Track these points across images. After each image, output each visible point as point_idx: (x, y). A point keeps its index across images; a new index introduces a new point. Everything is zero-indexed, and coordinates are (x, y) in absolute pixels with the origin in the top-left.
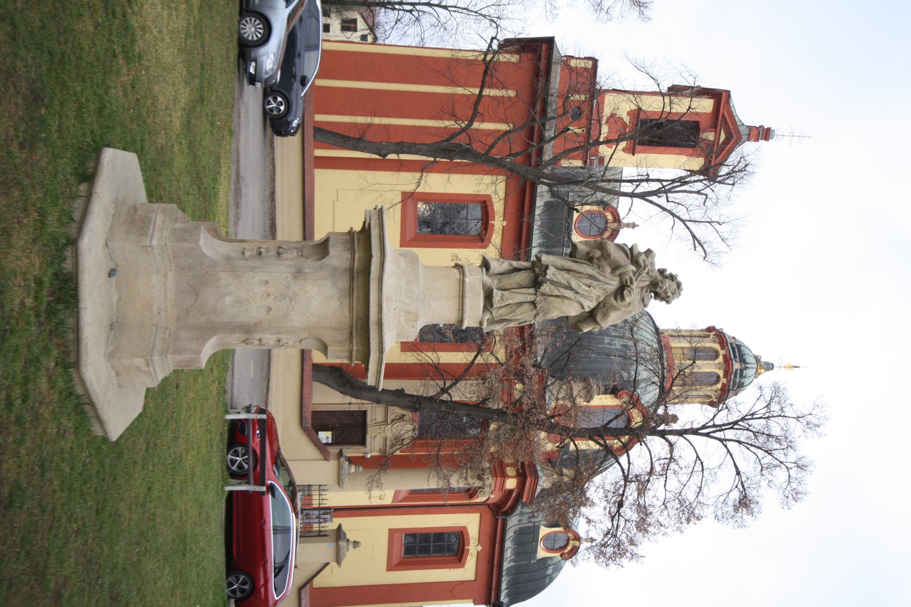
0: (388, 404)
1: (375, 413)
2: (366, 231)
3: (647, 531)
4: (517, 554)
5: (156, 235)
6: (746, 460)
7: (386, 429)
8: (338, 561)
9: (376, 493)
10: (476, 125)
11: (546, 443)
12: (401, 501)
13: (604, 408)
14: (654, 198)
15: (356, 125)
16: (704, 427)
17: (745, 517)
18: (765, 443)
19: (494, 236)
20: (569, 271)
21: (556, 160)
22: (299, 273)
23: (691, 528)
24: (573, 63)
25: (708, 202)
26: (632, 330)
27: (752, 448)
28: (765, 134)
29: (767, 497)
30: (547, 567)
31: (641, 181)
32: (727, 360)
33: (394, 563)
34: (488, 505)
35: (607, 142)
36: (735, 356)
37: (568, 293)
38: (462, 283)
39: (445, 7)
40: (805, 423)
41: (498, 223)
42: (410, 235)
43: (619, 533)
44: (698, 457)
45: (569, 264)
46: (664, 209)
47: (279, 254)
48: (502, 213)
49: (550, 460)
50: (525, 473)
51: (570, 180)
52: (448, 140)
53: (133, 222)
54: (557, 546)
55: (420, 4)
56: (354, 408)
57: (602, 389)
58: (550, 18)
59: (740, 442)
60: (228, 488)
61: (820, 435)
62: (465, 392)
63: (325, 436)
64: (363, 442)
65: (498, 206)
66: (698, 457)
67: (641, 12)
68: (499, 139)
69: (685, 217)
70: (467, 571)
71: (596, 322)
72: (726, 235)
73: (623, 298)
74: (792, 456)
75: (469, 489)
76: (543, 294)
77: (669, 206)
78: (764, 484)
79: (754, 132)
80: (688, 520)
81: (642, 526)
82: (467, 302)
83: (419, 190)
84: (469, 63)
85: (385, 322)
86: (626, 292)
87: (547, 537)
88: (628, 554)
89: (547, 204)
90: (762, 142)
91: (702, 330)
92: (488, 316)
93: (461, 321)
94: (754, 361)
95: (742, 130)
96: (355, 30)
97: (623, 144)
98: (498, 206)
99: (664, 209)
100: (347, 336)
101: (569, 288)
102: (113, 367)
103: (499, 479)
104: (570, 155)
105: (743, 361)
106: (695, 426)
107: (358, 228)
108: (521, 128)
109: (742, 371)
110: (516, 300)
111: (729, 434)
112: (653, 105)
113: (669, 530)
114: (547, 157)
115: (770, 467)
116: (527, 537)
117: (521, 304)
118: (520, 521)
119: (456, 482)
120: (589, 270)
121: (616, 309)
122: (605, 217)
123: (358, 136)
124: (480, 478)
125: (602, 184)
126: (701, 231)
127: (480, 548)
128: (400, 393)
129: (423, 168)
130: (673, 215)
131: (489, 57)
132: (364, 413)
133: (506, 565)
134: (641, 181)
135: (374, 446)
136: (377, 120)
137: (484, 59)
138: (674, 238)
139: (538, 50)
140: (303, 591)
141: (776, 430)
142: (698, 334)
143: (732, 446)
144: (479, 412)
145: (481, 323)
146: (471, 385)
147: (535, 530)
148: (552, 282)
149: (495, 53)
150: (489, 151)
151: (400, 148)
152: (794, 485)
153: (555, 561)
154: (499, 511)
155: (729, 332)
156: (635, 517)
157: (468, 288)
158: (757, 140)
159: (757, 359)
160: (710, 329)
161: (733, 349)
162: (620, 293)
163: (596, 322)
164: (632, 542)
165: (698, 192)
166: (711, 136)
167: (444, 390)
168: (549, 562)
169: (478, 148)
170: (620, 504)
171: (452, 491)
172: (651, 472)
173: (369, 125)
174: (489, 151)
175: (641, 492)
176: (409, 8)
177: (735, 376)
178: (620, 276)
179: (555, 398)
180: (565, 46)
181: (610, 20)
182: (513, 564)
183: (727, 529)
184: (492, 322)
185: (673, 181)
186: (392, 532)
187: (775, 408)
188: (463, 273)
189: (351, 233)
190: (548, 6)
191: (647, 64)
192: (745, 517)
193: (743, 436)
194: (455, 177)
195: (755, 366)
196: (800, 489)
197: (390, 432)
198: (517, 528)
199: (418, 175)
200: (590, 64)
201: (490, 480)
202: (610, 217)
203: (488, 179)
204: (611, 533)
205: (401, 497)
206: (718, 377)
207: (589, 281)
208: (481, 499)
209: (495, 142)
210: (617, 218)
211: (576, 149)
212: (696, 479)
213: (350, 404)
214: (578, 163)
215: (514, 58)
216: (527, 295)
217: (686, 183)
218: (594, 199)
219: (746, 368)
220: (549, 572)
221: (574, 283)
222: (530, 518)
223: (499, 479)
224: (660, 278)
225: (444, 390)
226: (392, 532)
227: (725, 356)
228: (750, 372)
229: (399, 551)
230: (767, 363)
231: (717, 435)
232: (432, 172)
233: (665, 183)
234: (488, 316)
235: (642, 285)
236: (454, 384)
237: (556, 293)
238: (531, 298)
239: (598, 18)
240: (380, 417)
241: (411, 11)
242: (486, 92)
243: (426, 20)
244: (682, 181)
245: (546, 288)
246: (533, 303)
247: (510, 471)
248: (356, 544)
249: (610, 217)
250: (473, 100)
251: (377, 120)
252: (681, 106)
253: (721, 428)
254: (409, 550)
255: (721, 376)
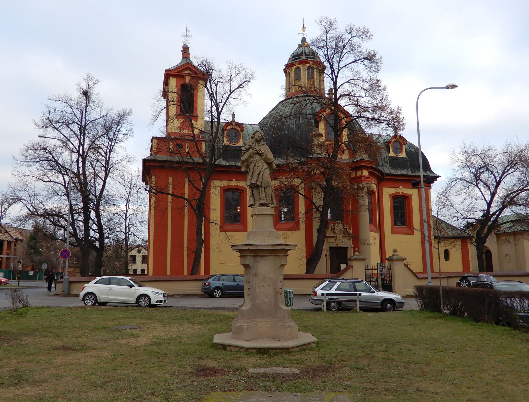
0: (325, 237)
1: (329, 243)
2: (239, 251)
3: (386, 106)
4: (404, 167)
5: (244, 325)
6: (348, 58)
7: (338, 237)
8: (403, 260)
9: (372, 241)
10: (186, 197)
11: (344, 157)
12: (377, 228)
13: (326, 129)
14: (220, 109)
15: (188, 255)
16: (333, 80)
17: (377, 58)
18: (339, 49)
19: (240, 185)
20: (252, 174)
21: (201, 155)
22: (255, 275)
23: (383, 84)
24: (155, 149)
25: (222, 80)
26: (284, 117)
27: (342, 55)
28: (186, 50)
29: (367, 46)
30: (411, 152)
31: (212, 115)
32: (301, 63)
33: (410, 231)
34: (378, 183)
35: (193, 131)
36: (299, 58)
37: (261, 175)
38: (258, 215)
39: (127, 211)
40: (329, 29)
41: (234, 183)
42: (241, 227)
43: (388, 120)
44: (347, 82)
45: (250, 175)
46: (225, 103)
47: (249, 282)
48: (229, 181)
49: (353, 153)
50: (357, 166)
51: (212, 149)
52: (195, 210)
53: (238, 332)
54: (400, 147)
55: (125, 224)
56: (328, 253)
57: (317, 129)
58: (132, 159)
59: (340, 61)
60: (358, 310)
61: (335, 21)
62: (318, 199)
63: (343, 267)
64: (346, 248)
65: (226, 183)
66: (347, 82)
67: (128, 114)
68: (194, 186)
69: (229, 93)
70: (413, 193)
71: (272, 162)
72: (237, 72)
73: (262, 153)
74: (346, 36)
75: (369, 194)
76: (261, 184)
77: (224, 101)
78: (359, 50)
79: (186, 55)
80: (379, 86)
81: (383, 108)
82: (265, 213)
83: (219, 223)
84: (157, 201)
85: (272, 244)
86: (260, 152)
87: (395, 152)
88: (398, 114)
89: (224, 160)
90: (190, 51)
91: (286, 76)
92: (270, 205)
93: (272, 215)
94: (301, 48)
95: (185, 62)
96: (135, 256)
97: (193, 122)
98: (226, 183)
99: (225, 103)
100: (278, 257)
101: (259, 174)
102: (290, 339)
103: (363, 179)
104: (199, 149)
105: (301, 54)
106: (332, 83)
107: (239, 254)
108: (187, 174)
109: (306, 55)
110: (264, 194)
111: (335, 66)
112: (173, 109)
113: (385, 94)
114: (200, 160)
115: (351, 46)
116: (395, 163)
117: (265, 192)
118: (386, 167)
119: (365, 201)
120: (252, 166)
121: (267, 155)
122: (230, 129)
123: (194, 254)
124: (363, 189)
125: (214, 135)
126: (235, 85)
127: (401, 187)
128: (319, 231)
129: (208, 222)
130: (228, 98)
131: (154, 191)
132: (331, 248)
133: (410, 173)
134: (212, 115)
135: (348, 243)
136: (186, 245)
137: (155, 194)
138: (239, 98)
139: (149, 166)
140: (419, 277)
141: (333, 44)
142: (288, 78)
143: (342, 64)
144: (329, 192)
145: (273, 207)
146: (315, 195)
147: (391, 158)
148: (257, 181)
149: (151, 187)
150: (200, 190)
151: (199, 233)
152: (361, 34)
153: (407, 148)
154: (382, 179)
155: (286, 62)
156: (378, 113)
157: (259, 213)
158: (189, 54)
159: (300, 46)
160: (285, 71)
161: (295, 60)
162: (261, 155)
163: (272, 162)
164: (392, 113)
165: (216, 86)
166: (188, 79)
167: (317, 209)
168: (408, 150)
169: (198, 196)
170: (373, 119)
171: (370, 203)
172: (356, 105)
173: (188, 248)
174: (200, 190)
175: (365, 109)
176: (127, 229)
177: (309, 58)
178: (254, 154)
179: (319, 153)
180: (147, 154)
181: (132, 130)
182: (409, 170)
183: (383, 67)
184: (272, 203)
185: (211, 100)
186: (393, 233)
187: (321, 44)
188: (254, 215)
189: (241, 256)
190: (126, 161)
191: (155, 114)
192: (377, 58)
193: (336, 59)
194: (212, 206)
195: (303, 47)
196: (362, 30)
197: (340, 235)
198: (390, 168)
199: (211, 224)
200: (155, 141)
201: (364, 184)
202: (229, 127)
203: (212, 190)
204: (388, 123)
205: (374, 228)
206: (309, 67)
207: (256, 167)
208: (375, 188)
209: (196, 187)
210: (230, 123)
211: (197, 147)
212: (358, 82)
213: (326, 255)
214: (203, 146)
215: (153, 177)
216: (262, 190)
217: (213, 94)
218: (221, 138)
219: (305, 52)
220: (413, 150)
221: (257, 173)
222: (385, 162)
223: (363, 179)
224: (254, 139)
225: (317, 209)
226: (393, 233)
227: (299, 64)
228: (307, 50)
229: (404, 229)
230: (302, 41)
231: (336, 71)
232: (210, 218)
233: (213, 104)
234: (270, 205)
235: (257, 146)
236: (314, 204)
237: (261, 179)
238: (263, 188)
239: (131, 136)
240: (333, 240)
241: (129, 228)
242: (170, 192)
243: (133, 221)
244: (211, 95)
245: (259, 183)
246: (265, 188)
247: (359, 173)
248: (395, 251)
249: (229, 127)
250: (175, 198)
251: (186, 245)
252: (173, 96)
253: (333, 70)
254: (403, 224)
255: (309, 65)
